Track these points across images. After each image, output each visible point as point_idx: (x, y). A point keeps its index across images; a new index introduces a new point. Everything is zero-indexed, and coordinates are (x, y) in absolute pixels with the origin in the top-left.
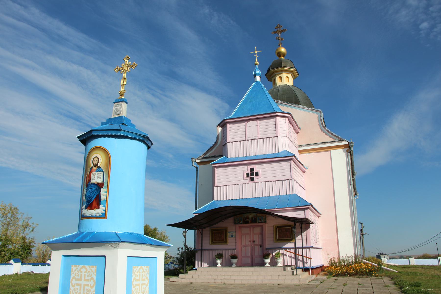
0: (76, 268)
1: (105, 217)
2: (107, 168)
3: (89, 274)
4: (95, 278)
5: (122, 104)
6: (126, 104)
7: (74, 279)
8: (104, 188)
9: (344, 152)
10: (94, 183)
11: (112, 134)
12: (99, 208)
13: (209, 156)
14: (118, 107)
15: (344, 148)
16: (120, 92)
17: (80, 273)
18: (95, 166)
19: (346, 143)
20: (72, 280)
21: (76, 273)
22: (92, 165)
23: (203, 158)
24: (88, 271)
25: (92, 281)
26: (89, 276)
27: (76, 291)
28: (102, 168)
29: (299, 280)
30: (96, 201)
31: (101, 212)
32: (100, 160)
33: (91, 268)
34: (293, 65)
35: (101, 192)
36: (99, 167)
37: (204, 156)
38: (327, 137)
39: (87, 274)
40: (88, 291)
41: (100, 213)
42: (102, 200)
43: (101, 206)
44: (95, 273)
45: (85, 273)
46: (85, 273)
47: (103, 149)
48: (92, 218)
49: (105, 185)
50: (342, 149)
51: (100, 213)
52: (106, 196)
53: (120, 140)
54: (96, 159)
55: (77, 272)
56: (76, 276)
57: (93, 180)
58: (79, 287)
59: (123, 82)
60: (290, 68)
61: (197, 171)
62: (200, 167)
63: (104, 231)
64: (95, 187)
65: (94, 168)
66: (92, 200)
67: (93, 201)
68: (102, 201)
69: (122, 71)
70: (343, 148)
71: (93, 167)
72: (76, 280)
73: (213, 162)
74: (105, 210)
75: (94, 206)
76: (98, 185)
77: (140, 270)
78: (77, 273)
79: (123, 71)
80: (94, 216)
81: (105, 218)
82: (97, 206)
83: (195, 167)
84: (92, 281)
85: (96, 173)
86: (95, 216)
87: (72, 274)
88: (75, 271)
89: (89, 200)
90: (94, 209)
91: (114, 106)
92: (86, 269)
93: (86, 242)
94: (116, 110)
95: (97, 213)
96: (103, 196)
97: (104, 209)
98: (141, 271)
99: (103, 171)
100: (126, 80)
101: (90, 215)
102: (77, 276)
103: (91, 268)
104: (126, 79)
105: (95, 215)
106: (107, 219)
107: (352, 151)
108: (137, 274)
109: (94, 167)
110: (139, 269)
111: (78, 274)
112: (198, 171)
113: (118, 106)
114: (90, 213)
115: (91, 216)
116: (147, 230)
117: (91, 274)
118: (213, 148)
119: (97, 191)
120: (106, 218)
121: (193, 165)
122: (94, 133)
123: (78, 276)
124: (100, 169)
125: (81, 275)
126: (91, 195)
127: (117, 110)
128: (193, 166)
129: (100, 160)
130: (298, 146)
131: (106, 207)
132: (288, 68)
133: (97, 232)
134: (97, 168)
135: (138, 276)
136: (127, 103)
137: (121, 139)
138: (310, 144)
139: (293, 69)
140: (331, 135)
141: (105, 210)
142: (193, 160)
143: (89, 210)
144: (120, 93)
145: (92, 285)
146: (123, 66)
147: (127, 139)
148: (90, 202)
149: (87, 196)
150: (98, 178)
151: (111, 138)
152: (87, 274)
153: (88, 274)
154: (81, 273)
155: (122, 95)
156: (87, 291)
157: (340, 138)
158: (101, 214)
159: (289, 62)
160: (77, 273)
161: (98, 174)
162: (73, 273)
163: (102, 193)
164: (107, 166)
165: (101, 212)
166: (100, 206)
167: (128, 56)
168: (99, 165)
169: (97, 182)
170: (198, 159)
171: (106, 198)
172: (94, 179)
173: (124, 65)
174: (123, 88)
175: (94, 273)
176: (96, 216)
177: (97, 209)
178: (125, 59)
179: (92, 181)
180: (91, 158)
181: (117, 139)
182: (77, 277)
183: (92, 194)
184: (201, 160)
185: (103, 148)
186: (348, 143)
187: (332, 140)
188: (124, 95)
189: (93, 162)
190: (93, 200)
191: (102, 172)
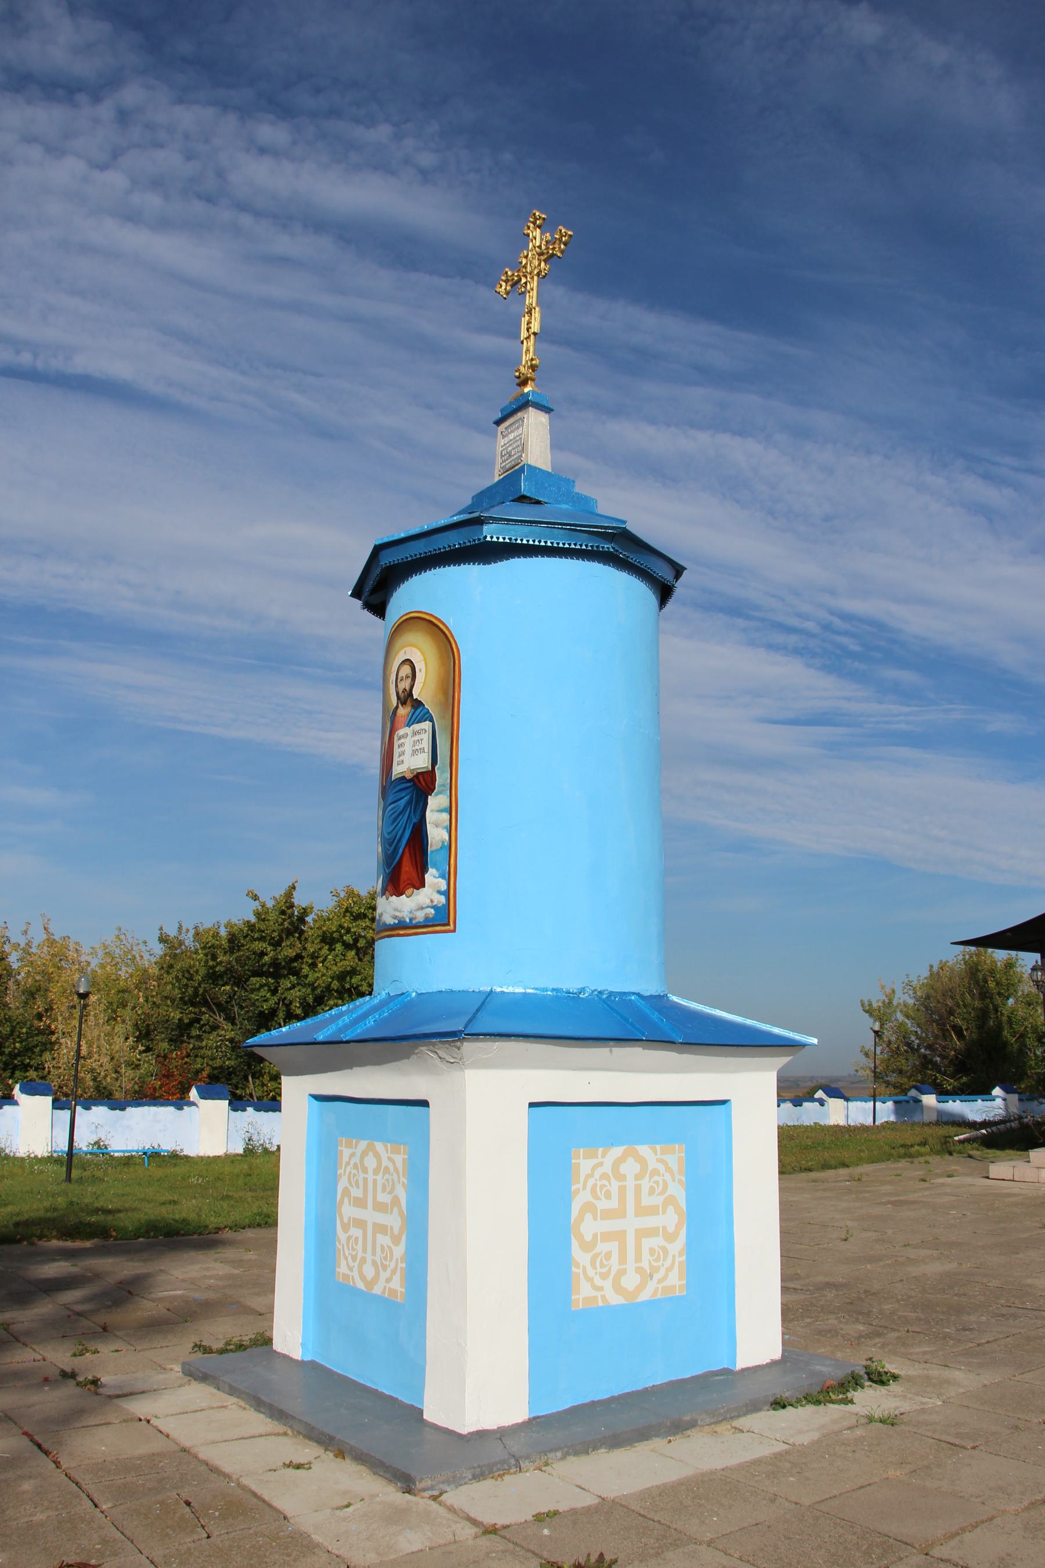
0: (593, 1162)
1: (448, 924)
2: (447, 699)
5: (526, 416)
6: (542, 414)
7: (588, 1216)
8: (437, 794)
10: (404, 778)
11: (450, 546)
12: (422, 884)
14: (511, 436)
16: (517, 374)
17: (614, 1186)
18: (404, 703)
20: (581, 1218)
25: (671, 1209)
26: (657, 1192)
27: (602, 1266)
28: (426, 706)
30: (412, 852)
31: (432, 901)
32: (420, 670)
33: (661, 1154)
35: (429, 814)
36: (418, 704)
39: (646, 1184)
41: (428, 907)
42: (434, 848)
43: (431, 875)
45: (638, 1182)
46: (638, 1182)
47: (425, 624)
49: (441, 777)
51: (428, 907)
52: (446, 828)
53: (493, 566)
54: (406, 670)
56: (597, 1198)
58: (613, 1246)
59: (527, 324)
63: (443, 987)
64: (408, 791)
65: (403, 711)
66: (398, 852)
68: (432, 852)
69: (523, 280)
71: (397, 707)
72: (599, 1218)
74: (447, 894)
75: (405, 878)
76: (418, 783)
77: (366, 1159)
78: (599, 1183)
79: (526, 283)
80: (408, 921)
82: (414, 875)
84: (671, 1209)
86: (411, 920)
87: (578, 1190)
90: (409, 891)
91: (499, 435)
92: (642, 1161)
93: (410, 1043)
94: (507, 448)
95: (419, 909)
96: (436, 834)
97: (444, 887)
98: (371, 1162)
99: (432, 720)
100: (537, 314)
102: (603, 1197)
104: (537, 309)
105: (411, 916)
106: (454, 931)
108: (355, 1175)
110: (364, 1154)
113: (512, 432)
115: (397, 922)
116: (979, 967)
117: (663, 1180)
119: (414, 812)
122: (388, 558)
123: (608, 1195)
124: (420, 709)
125: (622, 1190)
127: (510, 449)
129: (420, 670)
131: (450, 876)
133: (419, 995)
134: (409, 708)
135: (357, 1181)
136: (547, 410)
141: (447, 894)
144: (519, 377)
145: (671, 1229)
146: (524, 261)
147: (495, 562)
150: (414, 752)
152: (646, 1184)
153: (651, 1184)
155: (524, 383)
158: (432, 911)
160: (602, 1187)
161: (415, 733)
162: (580, 1186)
163: (430, 816)
164: (445, 692)
165: (432, 901)
166: (426, 876)
167: (537, 214)
168: (416, 695)
169: (412, 771)
171: (447, 838)
173: (526, 257)
174: (528, 350)
176: (414, 922)
178: (529, 228)
180: (391, 669)
182: (603, 1204)
185: (427, 617)
188: (533, 380)
189: (397, 686)
190: (401, 851)
191: (426, 725)
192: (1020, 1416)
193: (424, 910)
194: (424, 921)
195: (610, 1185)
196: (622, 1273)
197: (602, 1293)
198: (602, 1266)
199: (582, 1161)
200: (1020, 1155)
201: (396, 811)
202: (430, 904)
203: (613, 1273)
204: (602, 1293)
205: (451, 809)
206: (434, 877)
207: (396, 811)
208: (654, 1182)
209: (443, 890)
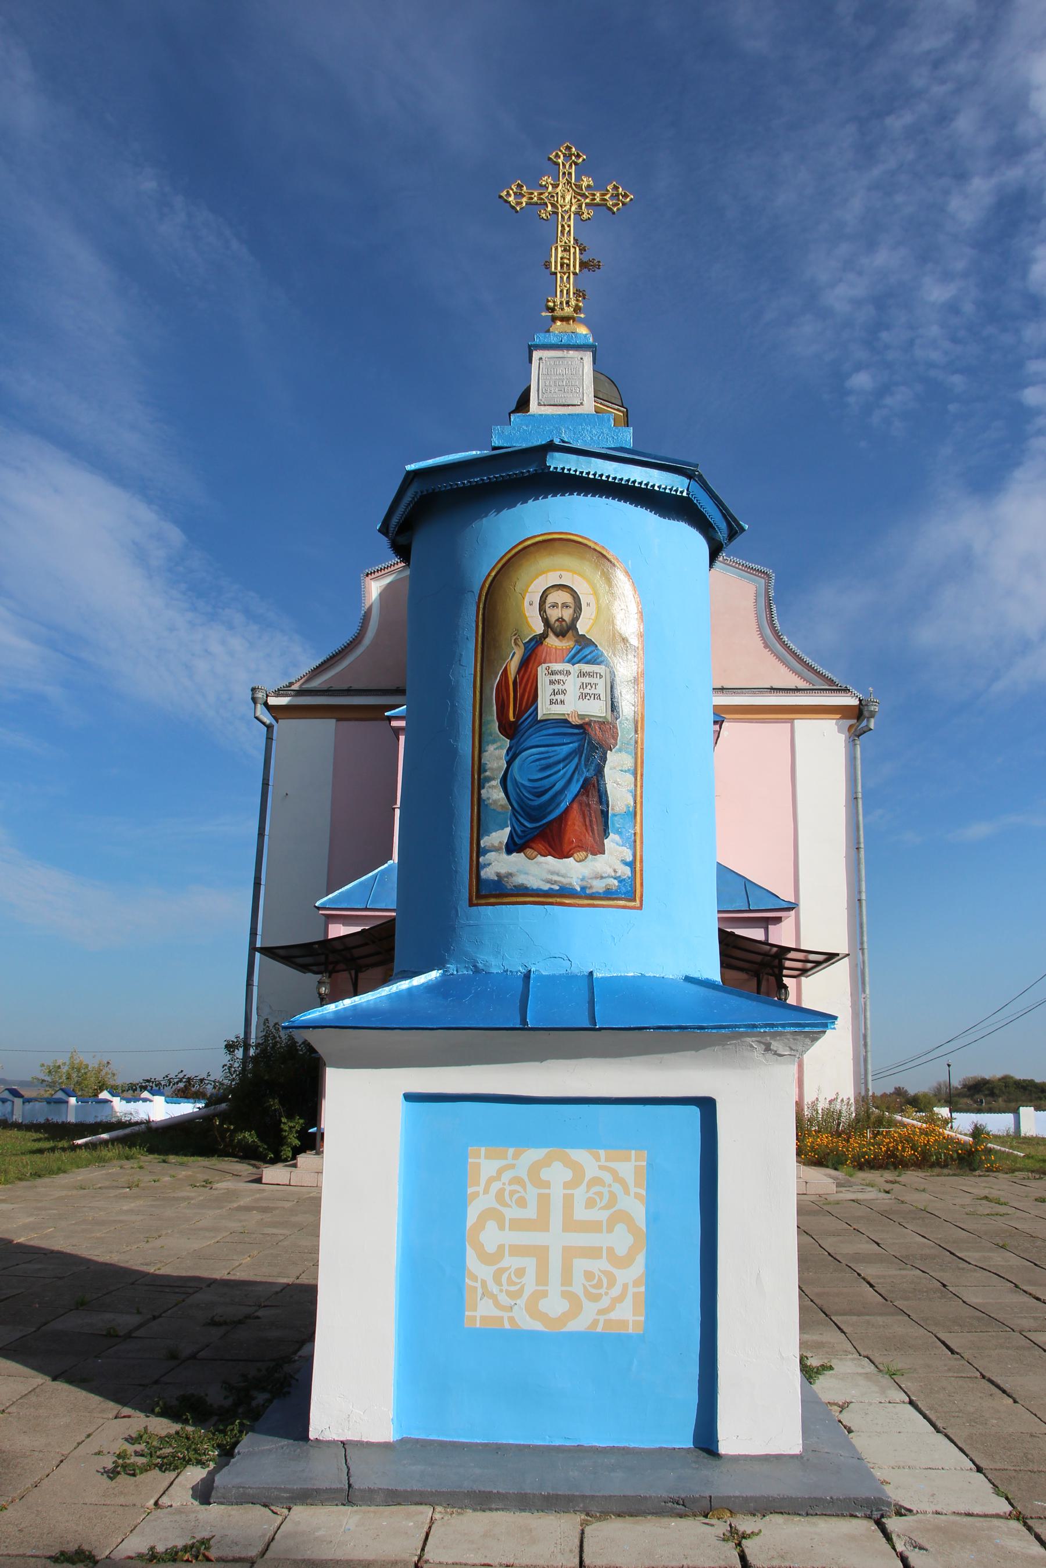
1: (634, 900)
3: (600, 1194)
4: (639, 1213)
9: (839, 732)
10: (566, 721)
13: (325, 687)
15: (840, 718)
18: (561, 634)
19: (852, 701)
21: (501, 1191)
22: (539, 628)
23: (300, 693)
24: (586, 1180)
29: (806, 1182)
31: (615, 871)
32: (588, 605)
33: (607, 1160)
34: (620, 397)
36: (584, 642)
37: (304, 687)
38: (783, 670)
39: (580, 1194)
40: (595, 1282)
44: (639, 1190)
48: (567, 901)
50: (835, 721)
51: (609, 877)
53: (667, 521)
55: (510, 1184)
57: (551, 703)
60: (610, 405)
61: (269, 739)
62: (284, 727)
64: (575, 738)
65: (552, 641)
66: (559, 804)
67: (567, 811)
70: (838, 716)
71: (544, 636)
73: (393, 712)
74: (632, 865)
78: (508, 1188)
80: (579, 889)
81: (632, 904)
83: (264, 723)
85: (568, 667)
86: (583, 888)
88: (498, 1176)
89: (536, 803)
92: (578, 1170)
95: (596, 878)
97: (629, 858)
101: (555, 882)
103: (607, 1160)
105: (584, 884)
106: (640, 908)
107: (871, 729)
109: (551, 634)
111: (516, 1196)
112: (274, 743)
114: (553, 873)
118: (343, 658)
120: (637, 904)
121: (258, 714)
122: (557, 462)
126: (542, 779)
128: (257, 718)
129: (588, 605)
130: (721, 690)
132: (601, 404)
134: (571, 644)
137: (676, 522)
138: (723, 689)
139: (618, 410)
140: (798, 667)
142: (260, 695)
143: (540, 858)
148: (544, 817)
149: (516, 783)
151: (632, 507)
152: (580, 1194)
153: (590, 1194)
154: (546, 1191)
156: (587, 1284)
157: (831, 682)
158: (616, 882)
159: (606, 384)
161: (582, 674)
162: (481, 1189)
168: (582, 627)
170: (278, 693)
171: (632, 803)
172: (559, 697)
175: (633, 1190)
176: (588, 891)
177: (590, 856)
179: (545, 708)
181: (657, 516)
183: (555, 777)
184: (290, 701)
186: (860, 701)
187: (802, 684)
192: (842, 1454)
193: (604, 880)
194: (604, 892)
195: (526, 1192)
196: (540, 1295)
197: (510, 1314)
198: (510, 1282)
199: (633, 1163)
200: (182, 1164)
201: (549, 757)
202: (613, 874)
203: (526, 1295)
204: (510, 1314)
205: (636, 772)
206: (617, 844)
207: (549, 757)
208: (595, 1193)
209: (628, 860)
